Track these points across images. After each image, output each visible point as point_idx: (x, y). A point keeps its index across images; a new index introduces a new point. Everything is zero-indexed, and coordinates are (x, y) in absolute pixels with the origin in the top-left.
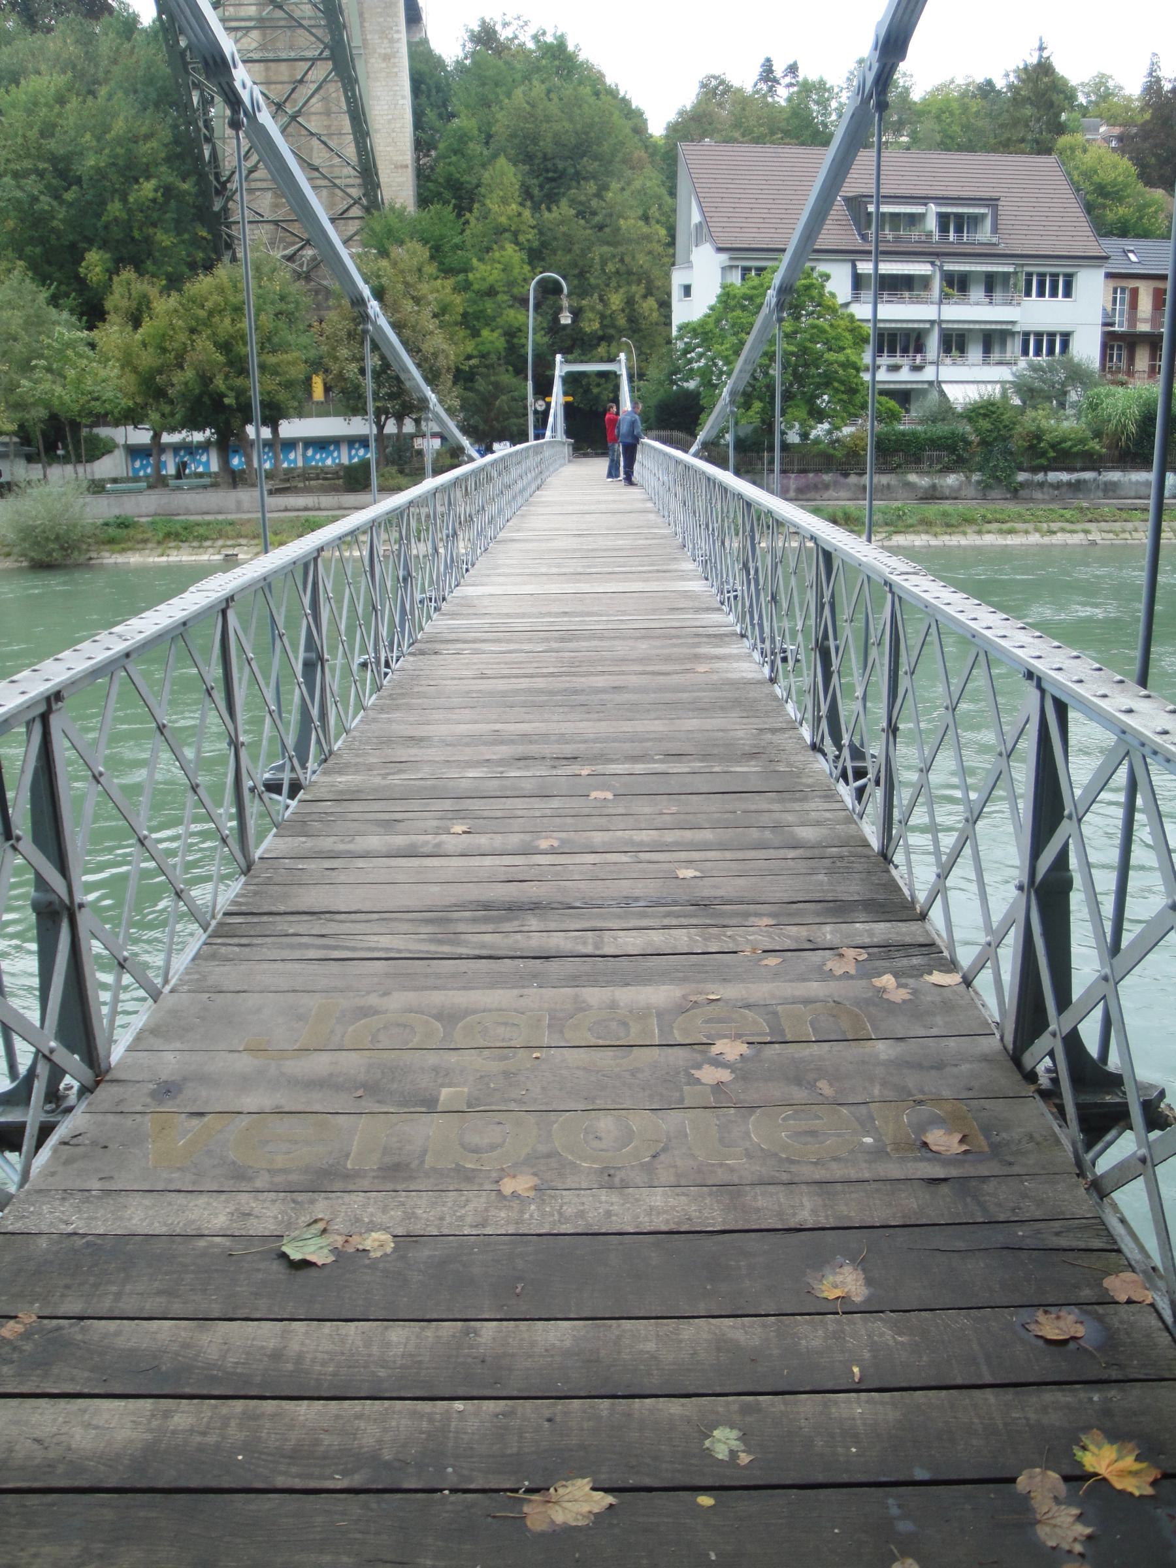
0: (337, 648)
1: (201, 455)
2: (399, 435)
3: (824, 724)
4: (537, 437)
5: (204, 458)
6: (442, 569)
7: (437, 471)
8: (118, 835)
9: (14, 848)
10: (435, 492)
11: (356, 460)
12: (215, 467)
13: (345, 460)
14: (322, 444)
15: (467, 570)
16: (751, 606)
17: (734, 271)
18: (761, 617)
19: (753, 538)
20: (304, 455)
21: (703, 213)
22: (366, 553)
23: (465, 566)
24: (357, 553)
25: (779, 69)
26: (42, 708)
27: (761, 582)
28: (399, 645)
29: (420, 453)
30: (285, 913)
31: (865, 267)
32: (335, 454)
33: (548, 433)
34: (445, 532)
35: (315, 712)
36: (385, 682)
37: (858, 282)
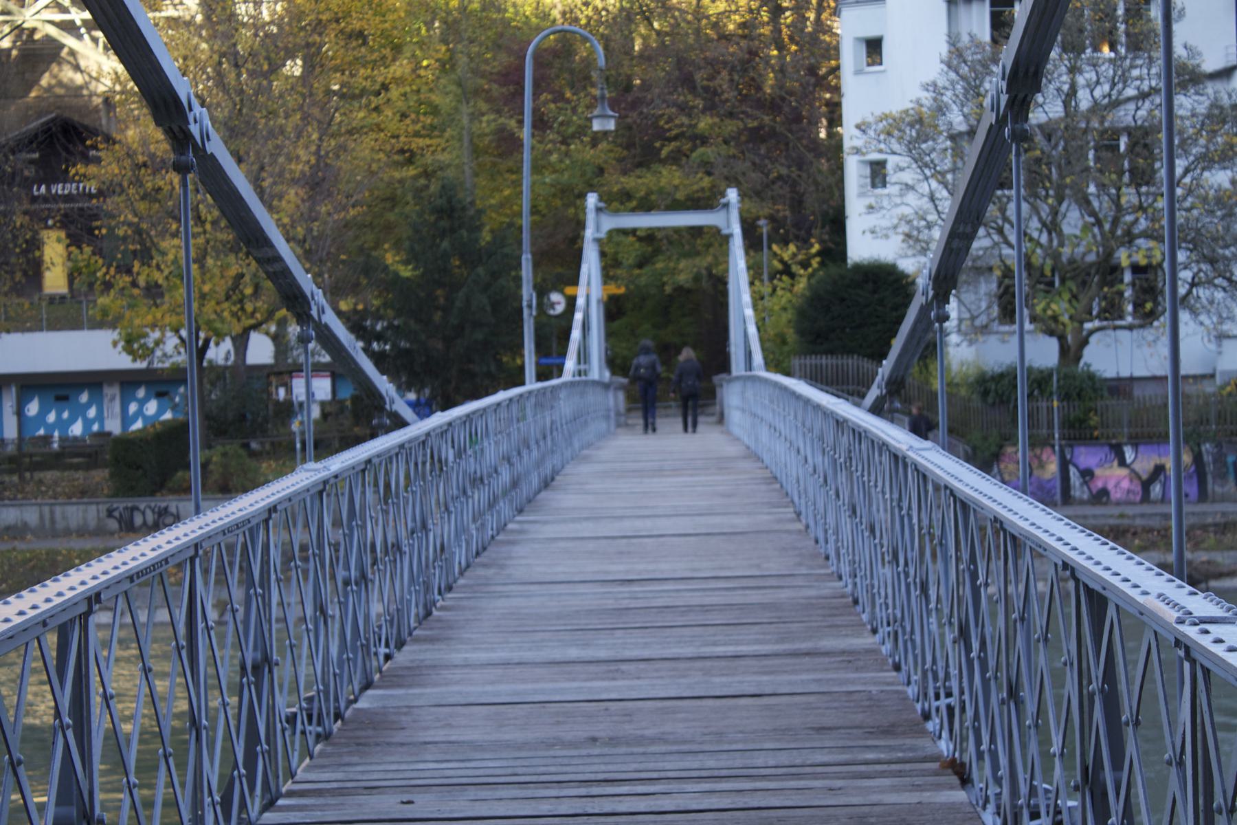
0: (157, 768)
2: (241, 372)
4: (542, 376)
6: (334, 650)
7: (324, 448)
10: (322, 490)
11: (138, 425)
13: (114, 426)
15: (388, 657)
16: (976, 716)
18: (993, 740)
19: (974, 576)
20: (20, 413)
22: (181, 616)
23: (383, 650)
24: (163, 615)
27: (992, 663)
28: (243, 806)
29: (287, 410)
32: (92, 412)
33: (570, 364)
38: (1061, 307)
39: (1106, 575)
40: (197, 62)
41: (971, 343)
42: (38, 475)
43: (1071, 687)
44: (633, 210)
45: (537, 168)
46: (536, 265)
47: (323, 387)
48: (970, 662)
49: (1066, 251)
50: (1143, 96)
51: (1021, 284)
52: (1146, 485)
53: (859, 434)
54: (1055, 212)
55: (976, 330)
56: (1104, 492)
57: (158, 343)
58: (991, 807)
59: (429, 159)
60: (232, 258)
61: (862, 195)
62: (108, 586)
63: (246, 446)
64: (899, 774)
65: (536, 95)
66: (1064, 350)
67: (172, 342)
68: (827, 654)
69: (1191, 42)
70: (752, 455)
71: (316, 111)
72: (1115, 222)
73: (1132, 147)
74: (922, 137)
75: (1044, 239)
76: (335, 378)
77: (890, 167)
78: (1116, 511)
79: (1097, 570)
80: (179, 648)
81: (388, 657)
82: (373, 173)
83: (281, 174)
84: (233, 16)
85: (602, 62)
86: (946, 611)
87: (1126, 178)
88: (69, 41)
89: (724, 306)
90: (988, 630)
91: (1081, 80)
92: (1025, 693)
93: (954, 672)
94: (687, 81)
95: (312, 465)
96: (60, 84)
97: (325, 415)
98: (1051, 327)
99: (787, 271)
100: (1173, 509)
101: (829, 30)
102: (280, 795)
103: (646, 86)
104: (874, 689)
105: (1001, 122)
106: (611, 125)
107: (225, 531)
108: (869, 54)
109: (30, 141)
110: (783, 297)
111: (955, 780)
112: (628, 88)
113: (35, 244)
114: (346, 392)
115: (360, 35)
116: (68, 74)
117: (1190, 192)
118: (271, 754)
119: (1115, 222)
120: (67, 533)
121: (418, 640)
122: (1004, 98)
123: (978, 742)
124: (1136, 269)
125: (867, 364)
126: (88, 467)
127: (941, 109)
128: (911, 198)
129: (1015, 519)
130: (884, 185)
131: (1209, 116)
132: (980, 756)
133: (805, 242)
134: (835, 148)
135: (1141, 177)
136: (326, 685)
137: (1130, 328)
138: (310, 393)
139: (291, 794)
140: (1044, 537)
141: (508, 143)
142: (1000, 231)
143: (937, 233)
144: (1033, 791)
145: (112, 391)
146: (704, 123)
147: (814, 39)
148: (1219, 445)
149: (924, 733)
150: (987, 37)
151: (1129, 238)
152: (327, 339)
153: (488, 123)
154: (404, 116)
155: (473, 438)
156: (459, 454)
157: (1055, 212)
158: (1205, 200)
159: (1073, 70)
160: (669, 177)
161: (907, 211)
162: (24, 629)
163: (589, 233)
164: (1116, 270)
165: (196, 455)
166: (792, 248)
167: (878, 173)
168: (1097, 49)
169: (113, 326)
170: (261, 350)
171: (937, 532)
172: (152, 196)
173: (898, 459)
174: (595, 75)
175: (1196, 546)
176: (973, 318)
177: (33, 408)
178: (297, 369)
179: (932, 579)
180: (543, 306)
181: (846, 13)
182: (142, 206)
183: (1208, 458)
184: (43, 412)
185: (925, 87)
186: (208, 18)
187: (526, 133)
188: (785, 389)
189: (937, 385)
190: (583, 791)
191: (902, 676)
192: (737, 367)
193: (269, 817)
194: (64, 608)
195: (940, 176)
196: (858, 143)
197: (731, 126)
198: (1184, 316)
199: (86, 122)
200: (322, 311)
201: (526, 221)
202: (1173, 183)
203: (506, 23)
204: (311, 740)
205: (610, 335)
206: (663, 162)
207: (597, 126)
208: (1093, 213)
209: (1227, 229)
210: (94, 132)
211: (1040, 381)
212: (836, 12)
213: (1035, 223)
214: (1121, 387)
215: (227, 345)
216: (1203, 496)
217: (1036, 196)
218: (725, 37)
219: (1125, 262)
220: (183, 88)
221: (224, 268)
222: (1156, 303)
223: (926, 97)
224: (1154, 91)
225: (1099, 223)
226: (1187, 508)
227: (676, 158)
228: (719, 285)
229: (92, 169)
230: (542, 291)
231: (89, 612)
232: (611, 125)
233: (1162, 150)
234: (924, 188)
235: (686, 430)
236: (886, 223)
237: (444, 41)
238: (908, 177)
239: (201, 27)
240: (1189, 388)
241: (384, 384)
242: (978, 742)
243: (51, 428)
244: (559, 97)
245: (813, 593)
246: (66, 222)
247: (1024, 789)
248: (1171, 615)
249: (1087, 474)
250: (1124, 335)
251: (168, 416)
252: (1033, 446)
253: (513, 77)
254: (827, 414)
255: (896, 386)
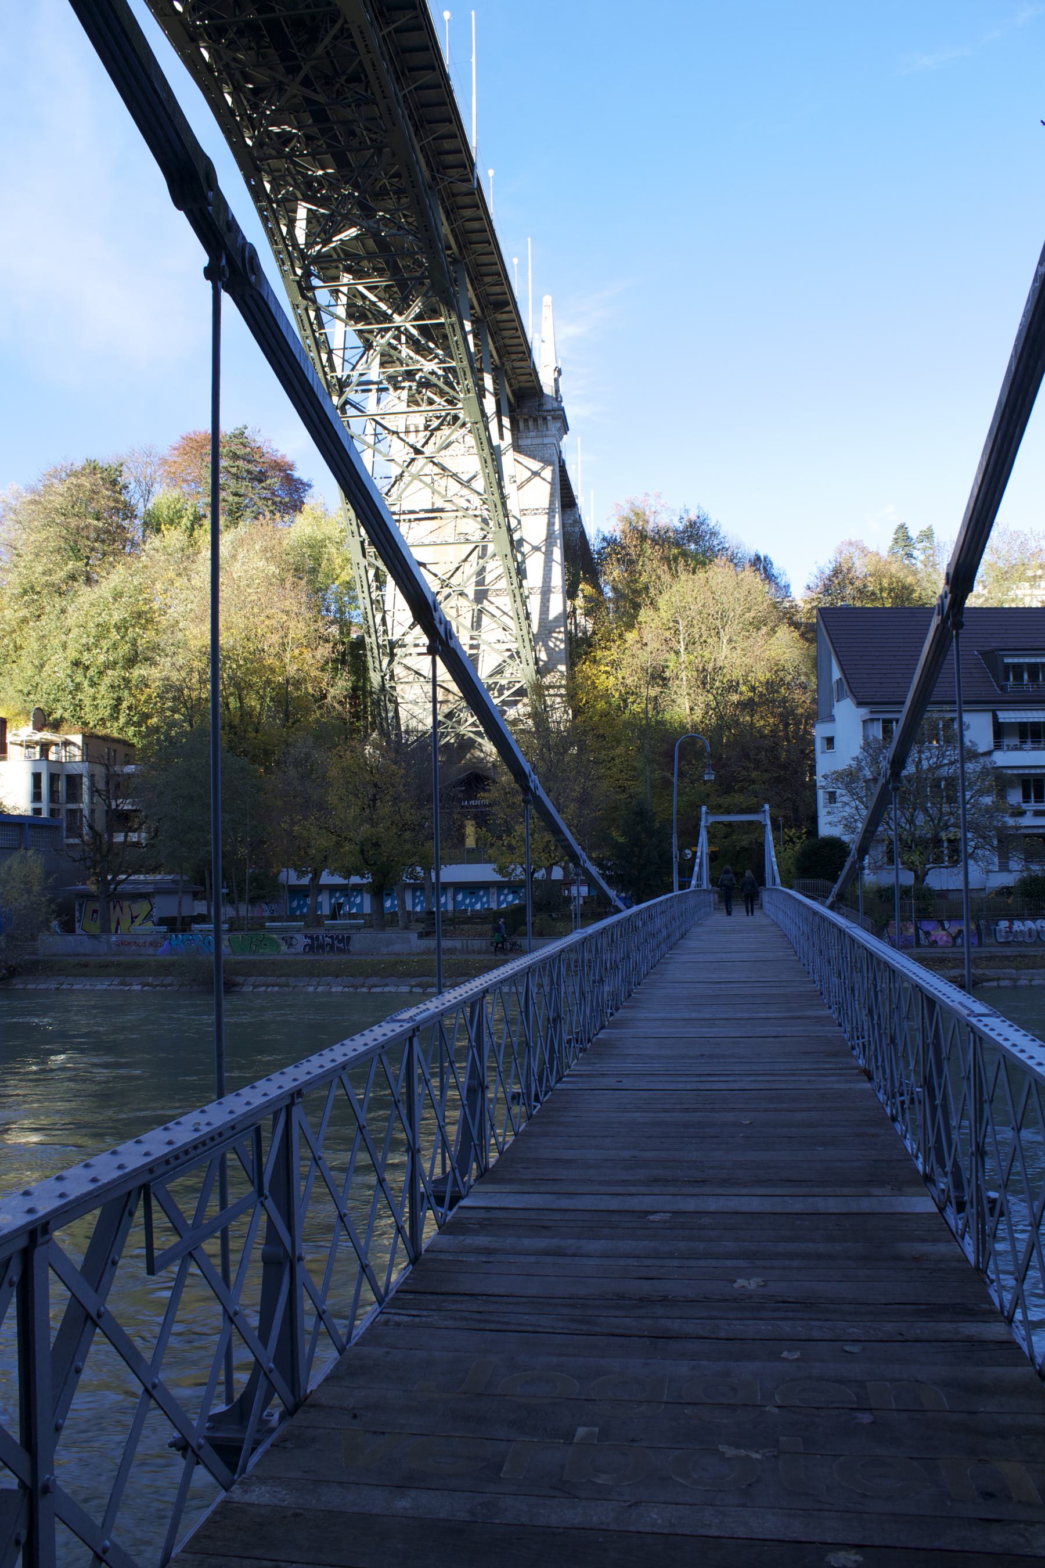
1: (356, 897)
2: (548, 882)
3: (933, 1158)
4: (681, 888)
5: (358, 900)
6: (588, 1012)
8: (430, 1107)
9: (263, 1205)
10: (584, 941)
11: (504, 906)
12: (367, 909)
13: (494, 906)
14: (472, 888)
15: (612, 1014)
17: (875, 723)
18: (883, 1061)
20: (454, 899)
21: (843, 670)
23: (609, 1011)
25: (914, 533)
26: (288, 1101)
27: (883, 1026)
28: (548, 1080)
29: (569, 900)
30: (454, 1294)
31: (1006, 716)
32: (485, 900)
33: (694, 882)
34: (592, 978)
35: (475, 1133)
36: (534, 1112)
37: (1000, 731)
38: (915, 858)
39: (935, 992)
40: (532, 747)
41: (875, 874)
42: (461, 926)
43: (919, 1040)
44: (722, 813)
45: (680, 794)
46: (679, 837)
47: (584, 890)
48: (873, 1025)
49: (918, 833)
50: (952, 763)
51: (897, 847)
52: (954, 939)
53: (824, 918)
54: (912, 815)
55: (877, 868)
56: (935, 942)
57: (513, 870)
58: (882, 1091)
59: (632, 791)
60: (545, 833)
61: (825, 807)
62: (492, 986)
63: (550, 916)
64: (840, 1075)
65: (679, 762)
66: (917, 877)
67: (519, 870)
68: (808, 1018)
69: (973, 740)
70: (775, 924)
71: (583, 770)
72: (940, 820)
73: (947, 786)
74: (852, 782)
75: (907, 827)
76: (589, 885)
77: (837, 794)
78: (940, 950)
79: (931, 989)
80: (521, 1012)
81: (612, 1014)
82: (607, 796)
83: (568, 797)
84: (548, 728)
85: (709, 749)
86: (862, 1001)
87: (944, 800)
88: (480, 740)
89: (763, 856)
90: (882, 1010)
91: (923, 756)
92: (898, 1041)
93: (866, 1027)
94: (747, 756)
95: (580, 931)
96: (475, 757)
97: (585, 903)
98: (911, 867)
99: (791, 840)
100: (965, 950)
101: (810, 734)
102: (564, 1076)
103: (728, 758)
104: (829, 1035)
105: (887, 782)
106: (713, 777)
107: (541, 961)
108: (830, 799)
109: (461, 782)
110: (789, 852)
111: (866, 1078)
112: (720, 759)
113: (462, 827)
114: (594, 893)
115: (603, 736)
116: (478, 753)
117: (973, 807)
118: (560, 1058)
119: (940, 820)
120: (473, 952)
121: (624, 1007)
122: (889, 772)
123: (877, 1062)
124: (949, 841)
125: (828, 883)
126: (482, 924)
127: (860, 769)
128: (847, 808)
129: (894, 963)
130: (835, 802)
131: (981, 772)
132: (877, 1067)
133: (799, 827)
134: (813, 785)
135: (951, 800)
136: (584, 1027)
137: (947, 867)
138: (579, 893)
139: (568, 1076)
140: (907, 972)
141: (667, 783)
142: (888, 823)
143: (860, 825)
144: (901, 1084)
145: (493, 891)
146: (754, 775)
147: (803, 737)
148: (987, 921)
149: (852, 1056)
150: (881, 737)
151: (946, 827)
152: (587, 872)
153: (658, 774)
154: (622, 771)
155: (651, 917)
156: (644, 924)
157: (912, 815)
158: (980, 809)
159: (920, 752)
160: (739, 798)
161: (845, 814)
162: (456, 1005)
163: (703, 823)
164: (940, 841)
165: (529, 919)
166: (794, 830)
167: (832, 797)
168: (930, 742)
169: (494, 862)
170: (557, 873)
171: (859, 965)
172: (512, 806)
173: (841, 931)
174: (706, 754)
175: (977, 967)
176: (875, 862)
177: (460, 897)
178: (573, 882)
179: (856, 987)
180: (682, 856)
181: (817, 726)
182: (507, 810)
183: (982, 927)
184: (464, 899)
185: (853, 759)
186: (537, 729)
187: (675, 779)
188: (790, 895)
189: (859, 893)
190: (697, 1079)
191: (842, 1029)
192: (769, 884)
193: (559, 1086)
194: (473, 995)
195: (860, 799)
196: (823, 784)
197: (766, 776)
198: (971, 862)
199: (485, 774)
200: (585, 862)
201: (675, 818)
202: (965, 803)
203: (667, 730)
204: (578, 1051)
205: (711, 868)
206: (735, 791)
207: (706, 778)
208: (930, 816)
209: (990, 823)
210: (487, 778)
211: (906, 891)
212: (813, 726)
213: (903, 821)
214: (943, 894)
215: (543, 871)
216: (980, 944)
217: (904, 808)
218: (763, 737)
219: (944, 838)
220: (527, 767)
221: (543, 837)
222: (959, 856)
223: (854, 763)
224: (956, 761)
225: (932, 820)
226: (972, 950)
227: (741, 790)
228: (761, 846)
229: (487, 795)
230: (681, 849)
231: (484, 997)
232: (713, 777)
233: (960, 788)
234: (853, 804)
235: (748, 913)
236: (836, 820)
237: (639, 738)
238: (845, 799)
239: (534, 733)
240: (974, 895)
241: (612, 893)
242: (877, 1062)
243: (467, 905)
244: (689, 763)
245: (802, 989)
246: (475, 817)
247: (897, 1084)
248: (965, 1012)
249: (927, 934)
250: (944, 870)
251: (517, 902)
252: (902, 920)
253: (669, 755)
254: (808, 908)
255: (841, 897)
